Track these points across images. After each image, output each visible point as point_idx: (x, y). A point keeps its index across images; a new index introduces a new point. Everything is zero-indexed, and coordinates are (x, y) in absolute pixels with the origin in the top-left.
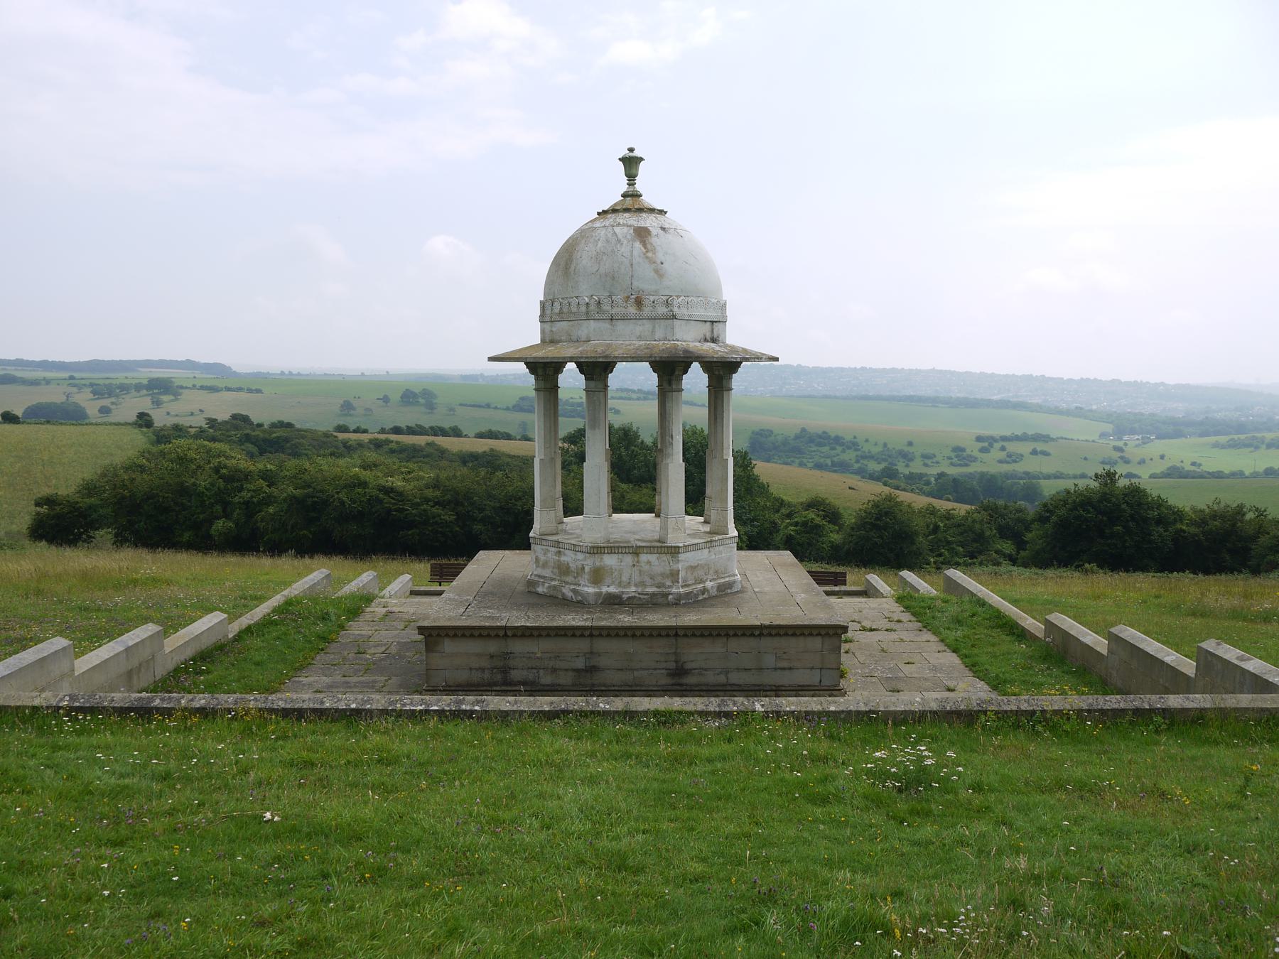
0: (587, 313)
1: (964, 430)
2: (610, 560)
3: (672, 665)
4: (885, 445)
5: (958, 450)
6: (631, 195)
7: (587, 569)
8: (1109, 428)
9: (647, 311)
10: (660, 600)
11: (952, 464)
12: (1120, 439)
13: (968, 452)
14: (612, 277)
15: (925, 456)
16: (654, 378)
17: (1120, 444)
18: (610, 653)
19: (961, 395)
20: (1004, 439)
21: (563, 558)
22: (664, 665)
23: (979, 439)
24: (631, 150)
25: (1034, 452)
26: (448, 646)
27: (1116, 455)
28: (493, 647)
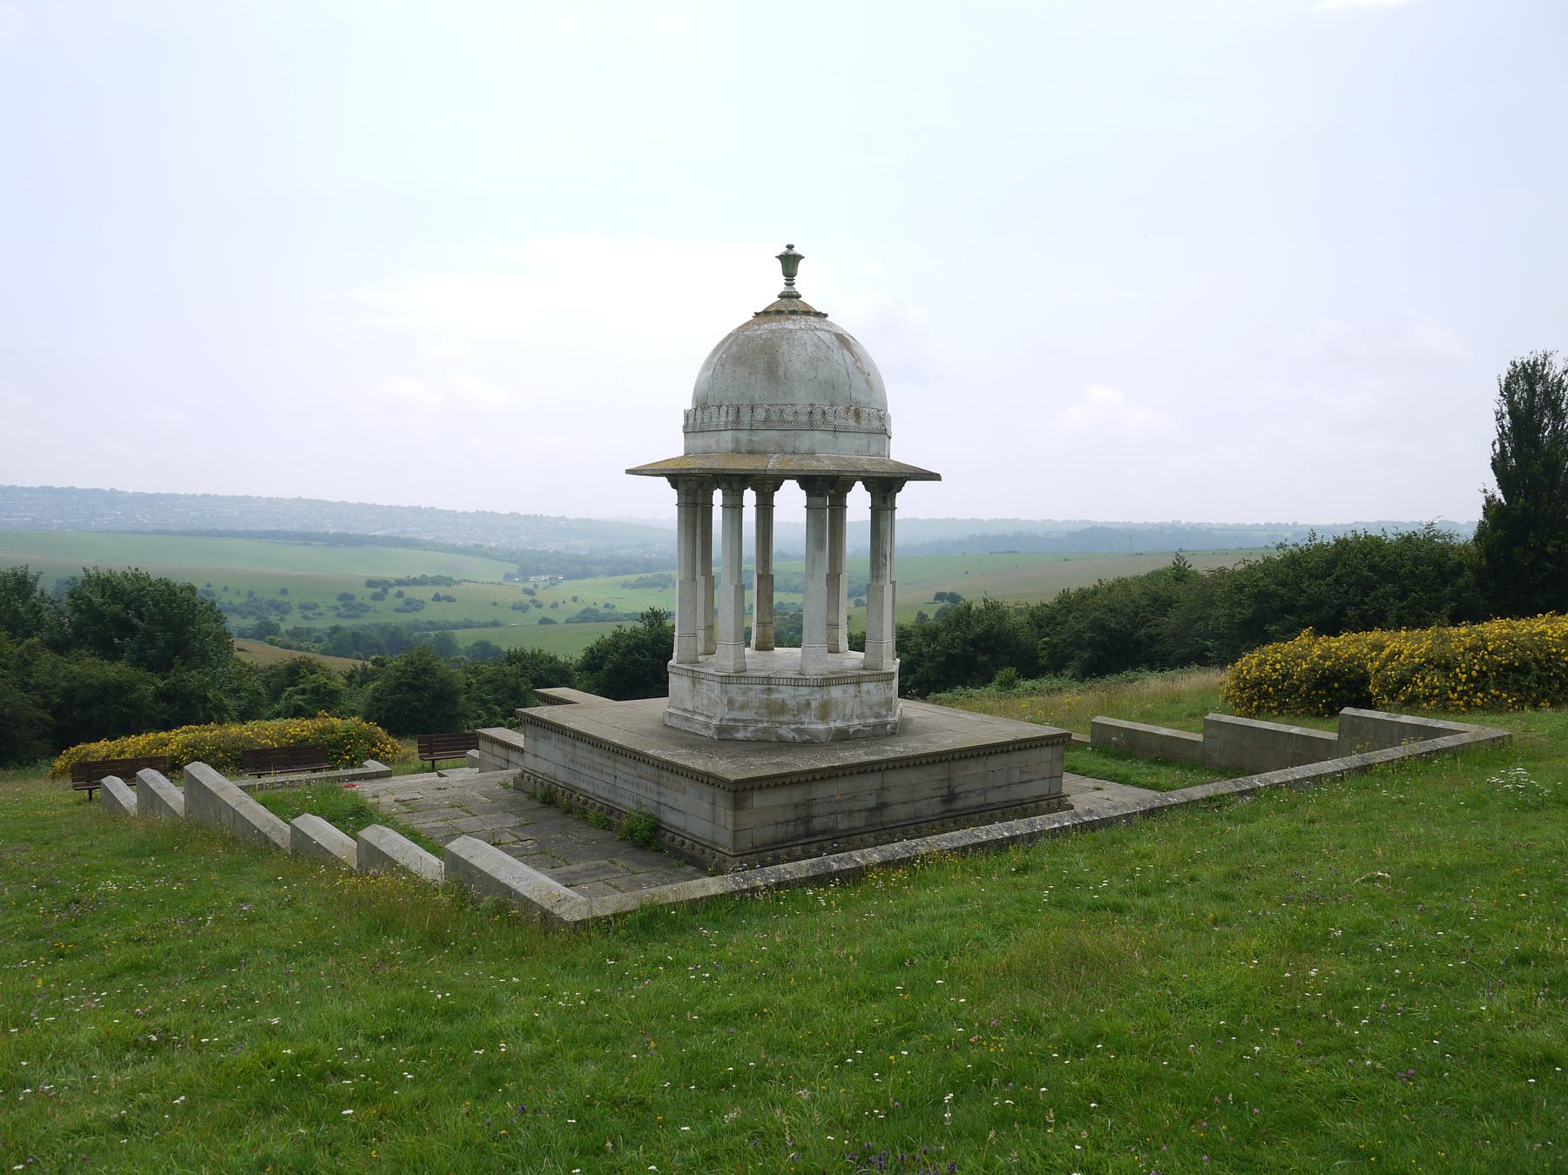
0: (811, 423)
1: (354, 570)
2: (836, 692)
3: (945, 792)
4: (251, 594)
5: (346, 598)
6: (790, 296)
7: (814, 704)
8: (513, 568)
9: (864, 424)
10: (880, 731)
11: (339, 615)
12: (526, 580)
13: (358, 600)
14: (831, 386)
15: (304, 607)
16: (673, 495)
17: (530, 586)
18: (968, 777)
19: (339, 530)
20: (400, 583)
21: (774, 696)
22: (939, 792)
23: (370, 584)
24: (790, 247)
25: (437, 598)
26: (759, 800)
27: (527, 599)
28: (797, 795)
